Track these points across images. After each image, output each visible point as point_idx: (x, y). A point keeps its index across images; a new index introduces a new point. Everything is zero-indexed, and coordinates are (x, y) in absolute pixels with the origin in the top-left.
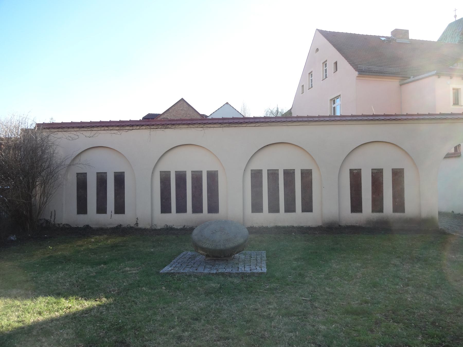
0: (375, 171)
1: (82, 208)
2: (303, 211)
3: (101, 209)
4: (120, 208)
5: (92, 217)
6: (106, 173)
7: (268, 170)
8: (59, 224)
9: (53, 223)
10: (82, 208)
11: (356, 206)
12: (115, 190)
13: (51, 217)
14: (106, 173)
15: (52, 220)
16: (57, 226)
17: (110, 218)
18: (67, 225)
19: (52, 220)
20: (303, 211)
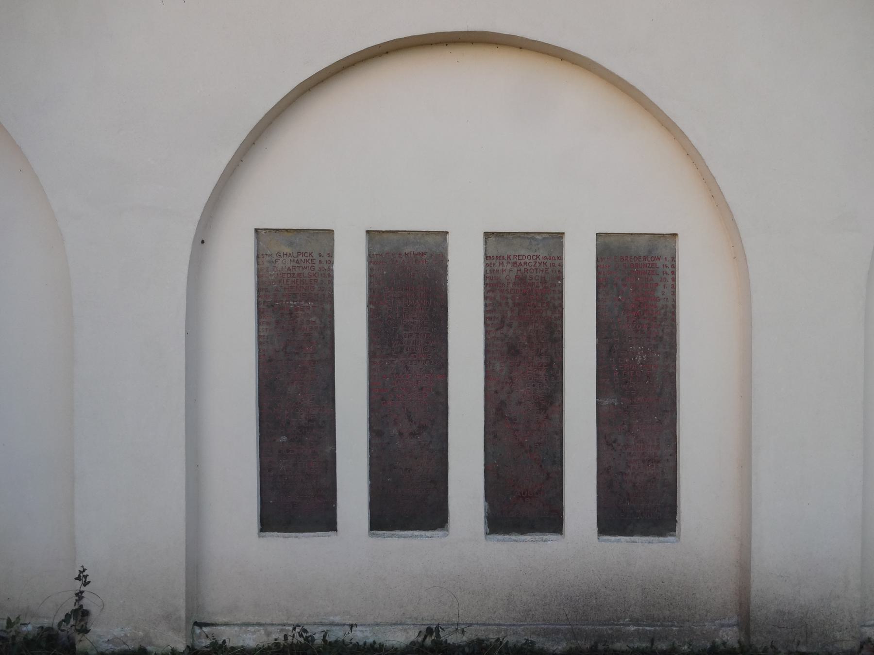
9: (735, 629)
11: (294, 497)
20: (386, 515)
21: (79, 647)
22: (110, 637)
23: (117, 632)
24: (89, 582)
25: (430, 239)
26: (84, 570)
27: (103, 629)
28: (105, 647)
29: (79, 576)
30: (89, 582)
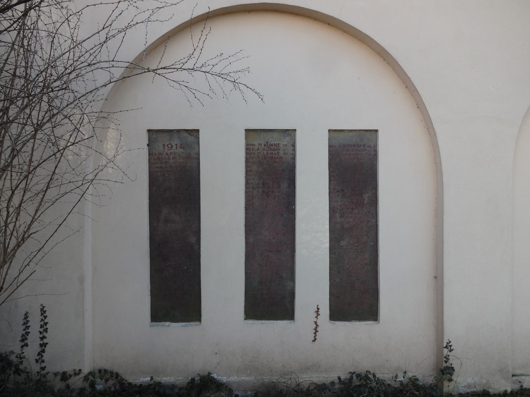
0: (257, 141)
1: (175, 291)
2: (338, 313)
3: (269, 298)
4: (356, 294)
5: (224, 330)
6: (290, 133)
7: (248, 132)
8: (65, 376)
9: (36, 368)
10: (175, 291)
12: (332, 211)
13: (24, 338)
14: (290, 133)
15: (31, 352)
16: (59, 385)
17: (313, 338)
18: (104, 373)
19: (31, 352)
20: (338, 313)
21: (446, 390)
22: (465, 384)
23: (470, 380)
24: (453, 350)
25: (273, 139)
26: (450, 342)
27: (464, 379)
28: (463, 390)
29: (447, 346)
30: (453, 350)
